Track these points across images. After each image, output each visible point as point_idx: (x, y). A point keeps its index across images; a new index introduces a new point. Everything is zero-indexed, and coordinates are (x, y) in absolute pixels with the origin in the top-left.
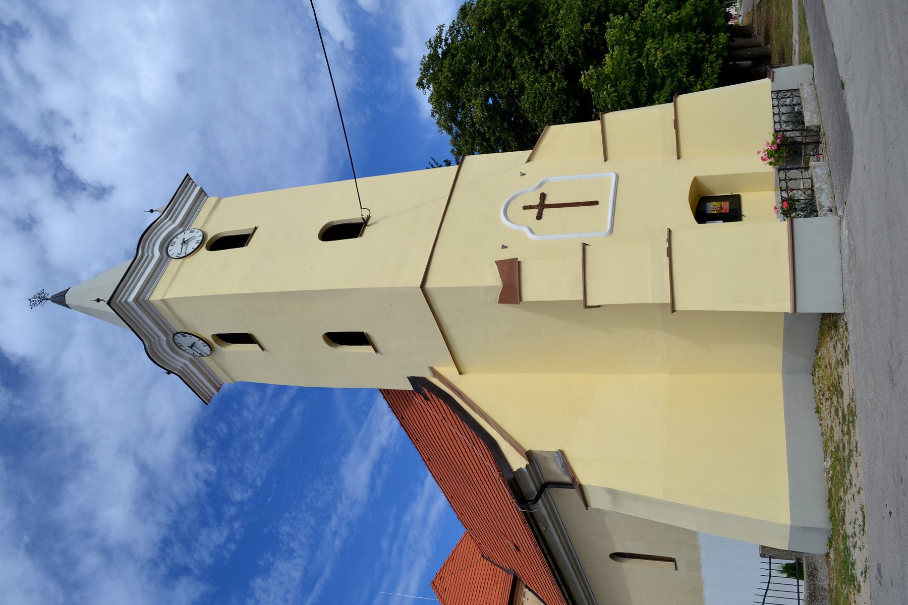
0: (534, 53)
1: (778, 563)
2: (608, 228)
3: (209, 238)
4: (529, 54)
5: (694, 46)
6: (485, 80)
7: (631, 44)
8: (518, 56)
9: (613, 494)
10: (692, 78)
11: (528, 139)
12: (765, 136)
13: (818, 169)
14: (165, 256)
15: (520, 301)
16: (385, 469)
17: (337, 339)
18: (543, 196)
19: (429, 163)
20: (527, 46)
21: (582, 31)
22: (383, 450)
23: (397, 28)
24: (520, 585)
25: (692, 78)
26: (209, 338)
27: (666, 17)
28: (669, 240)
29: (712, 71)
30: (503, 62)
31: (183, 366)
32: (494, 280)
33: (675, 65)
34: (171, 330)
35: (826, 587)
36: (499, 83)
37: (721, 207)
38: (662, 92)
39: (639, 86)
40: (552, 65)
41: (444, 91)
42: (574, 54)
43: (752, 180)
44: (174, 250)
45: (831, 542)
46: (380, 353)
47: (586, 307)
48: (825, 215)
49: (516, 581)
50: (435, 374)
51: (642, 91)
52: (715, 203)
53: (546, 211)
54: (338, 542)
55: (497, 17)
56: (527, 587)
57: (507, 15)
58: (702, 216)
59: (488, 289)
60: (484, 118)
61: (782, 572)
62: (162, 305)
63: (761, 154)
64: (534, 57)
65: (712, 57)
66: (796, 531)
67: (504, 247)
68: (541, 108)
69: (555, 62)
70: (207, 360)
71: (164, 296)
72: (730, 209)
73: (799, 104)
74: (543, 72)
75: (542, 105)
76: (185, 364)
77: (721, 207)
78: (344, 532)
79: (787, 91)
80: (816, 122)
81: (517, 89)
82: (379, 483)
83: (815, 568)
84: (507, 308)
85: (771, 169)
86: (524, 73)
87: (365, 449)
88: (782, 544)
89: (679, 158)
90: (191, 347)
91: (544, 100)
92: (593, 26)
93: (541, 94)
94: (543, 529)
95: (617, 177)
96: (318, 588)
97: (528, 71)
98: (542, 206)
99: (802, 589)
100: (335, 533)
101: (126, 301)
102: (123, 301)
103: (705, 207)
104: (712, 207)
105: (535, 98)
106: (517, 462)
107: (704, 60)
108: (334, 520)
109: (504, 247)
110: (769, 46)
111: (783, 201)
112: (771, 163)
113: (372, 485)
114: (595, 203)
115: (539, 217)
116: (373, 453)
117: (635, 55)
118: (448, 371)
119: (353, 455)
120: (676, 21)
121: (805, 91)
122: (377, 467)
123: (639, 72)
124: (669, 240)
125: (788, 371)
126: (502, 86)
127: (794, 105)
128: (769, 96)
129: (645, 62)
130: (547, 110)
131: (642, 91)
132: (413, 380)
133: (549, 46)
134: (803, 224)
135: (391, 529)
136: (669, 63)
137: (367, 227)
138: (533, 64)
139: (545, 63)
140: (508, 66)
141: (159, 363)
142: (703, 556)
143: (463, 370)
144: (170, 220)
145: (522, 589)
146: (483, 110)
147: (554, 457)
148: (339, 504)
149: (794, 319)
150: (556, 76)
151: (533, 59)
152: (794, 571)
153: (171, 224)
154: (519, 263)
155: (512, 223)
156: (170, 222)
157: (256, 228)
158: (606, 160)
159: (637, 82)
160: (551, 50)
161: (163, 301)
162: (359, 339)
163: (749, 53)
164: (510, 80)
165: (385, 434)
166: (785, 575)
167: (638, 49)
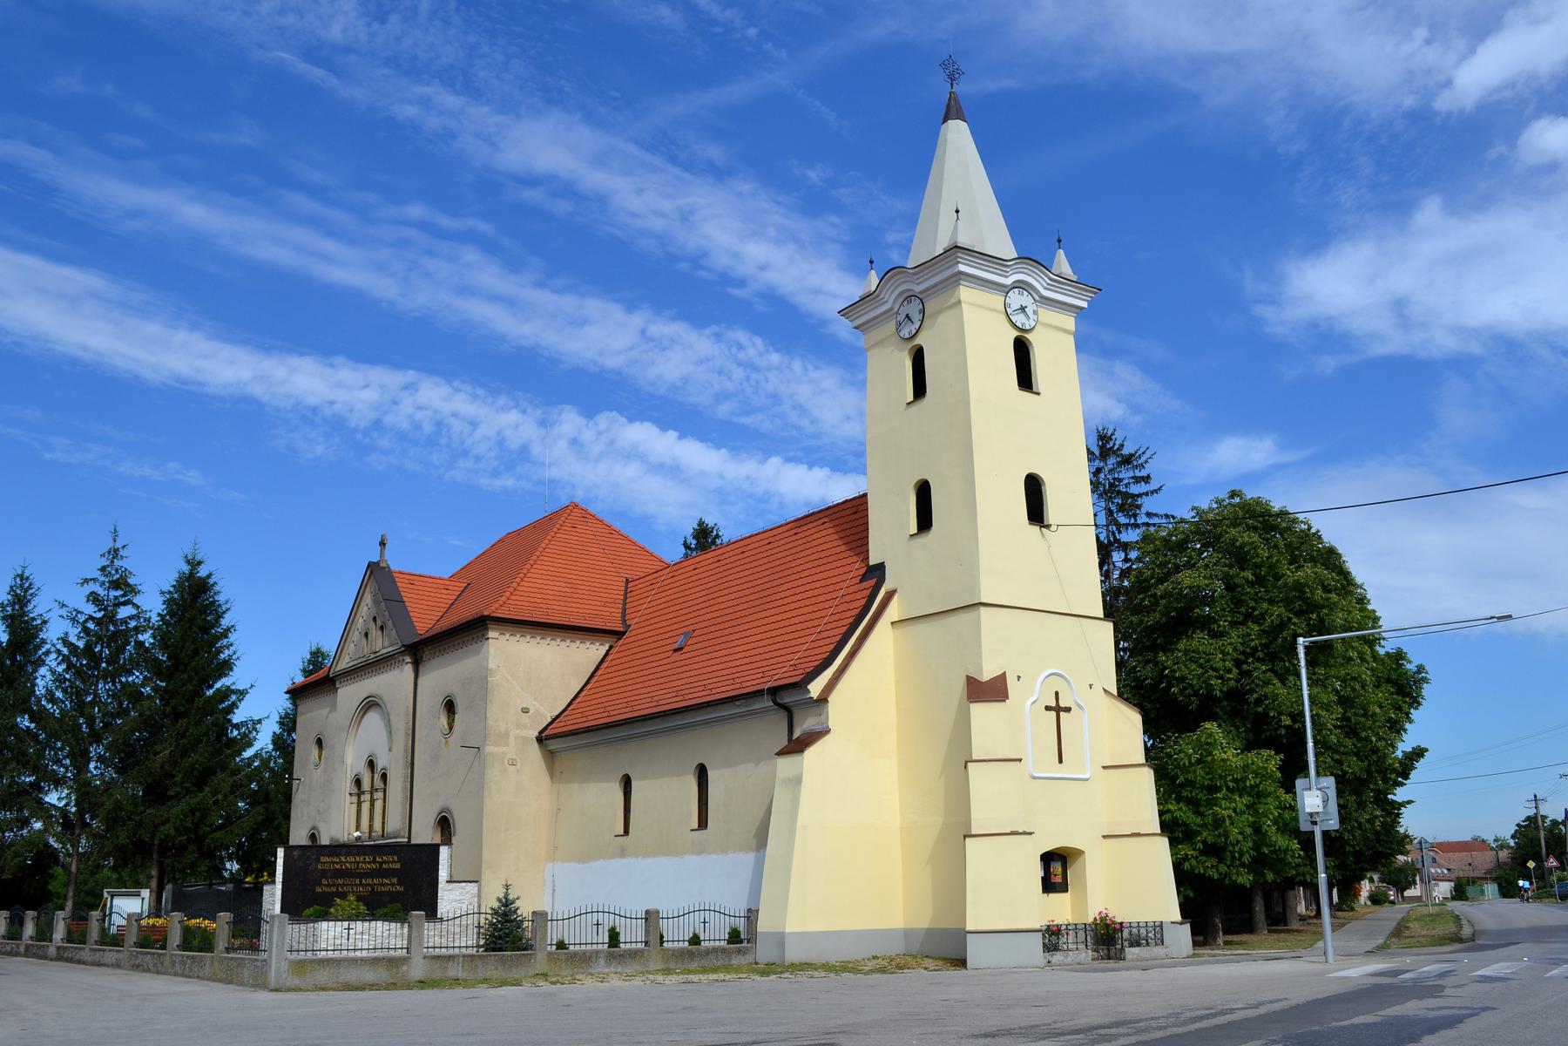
0: (1262, 651)
1: (741, 925)
2: (1037, 775)
3: (1026, 336)
4: (1261, 644)
5: (1237, 849)
6: (1230, 587)
7: (1244, 780)
8: (1260, 630)
9: (797, 781)
10: (1200, 846)
11: (1157, 638)
12: (1122, 913)
13: (1086, 955)
14: (1005, 290)
15: (971, 702)
16: (563, 207)
17: (924, 492)
18: (1068, 710)
19: (1148, 448)
20: (1271, 642)
21: (1281, 713)
22: (601, 200)
23: (1483, 203)
24: (613, 640)
25: (1200, 846)
26: (918, 341)
27: (1269, 819)
28: (1025, 833)
29: (1207, 867)
30: (1254, 609)
31: (885, 300)
32: (987, 674)
33: (1216, 828)
34: (927, 296)
35: (732, 962)
36: (1228, 604)
37: (1056, 875)
38: (1190, 814)
39: (1197, 788)
40: (1248, 674)
41: (1221, 533)
42: (1259, 701)
43: (1081, 901)
44: (1016, 299)
45: (772, 965)
46: (909, 540)
47: (966, 762)
48: (1045, 958)
49: (619, 635)
50: (890, 595)
51: (1191, 792)
52: (1060, 869)
53: (1053, 714)
54: (410, 111)
55: (1308, 604)
56: (611, 647)
57: (1310, 619)
58: (1048, 858)
59: (980, 668)
60: (1181, 588)
61: (731, 928)
62: (953, 301)
63: (1105, 911)
64: (1258, 651)
65: (1223, 868)
66: (780, 939)
67: (1019, 677)
68: (1191, 660)
69: (1250, 677)
70: (890, 327)
71: (965, 303)
72: (1055, 883)
73: (1148, 944)
74: (1238, 663)
75: (1194, 662)
76: (886, 302)
77: (1056, 875)
78: (433, 123)
79: (1162, 936)
80: (1129, 957)
81: (1218, 628)
82: (533, 196)
83: (745, 954)
84: (960, 686)
85: (1090, 920)
86: (1239, 637)
87: (601, 160)
88: (763, 925)
89: (1104, 837)
90: (907, 316)
91: (1201, 666)
92: (1287, 727)
93: (1209, 661)
94: (737, 703)
95: (1087, 780)
96: (317, 73)
97: (1240, 643)
98: (1058, 710)
99: (681, 944)
100: (426, 103)
101: (958, 262)
102: (959, 260)
103: (1057, 861)
104: (1057, 868)
105: (1205, 653)
106: (815, 688)
107: (1221, 860)
108: (452, 101)
109: (1019, 677)
110: (1266, 932)
111: (1057, 926)
112: (1095, 919)
113: (530, 180)
114: (1061, 761)
115: (1048, 708)
116: (595, 179)
117: (1231, 784)
118: (893, 612)
119: (587, 137)
120: (1263, 831)
121: (1160, 950)
122: (568, 189)
123: (1213, 789)
124: (1025, 833)
125: (908, 933)
126: (1224, 610)
127: (1147, 940)
128: (1158, 919)
129: (1221, 796)
130: (1188, 668)
131: (1191, 792)
132: (880, 568)
133: (1269, 670)
134: (1037, 941)
135: (446, 222)
136: (1218, 823)
137: (1039, 528)
138: (1248, 650)
139: (1249, 664)
140: (1248, 616)
141: (887, 276)
142: (714, 856)
143: (895, 626)
144: (1048, 284)
145: (607, 642)
146: (1190, 588)
147: (822, 724)
148: (486, 109)
149: (961, 935)
150: (1230, 679)
151: (1255, 649)
152: (734, 936)
153: (1043, 286)
154: (1005, 701)
155: (1046, 677)
156: (1045, 285)
157: (1038, 394)
158: (1104, 767)
159: (1203, 787)
160: (1264, 672)
161: (959, 302)
162: (925, 521)
163: (1257, 909)
164: (1229, 619)
165: (635, 203)
166: (691, 935)
167: (1238, 788)
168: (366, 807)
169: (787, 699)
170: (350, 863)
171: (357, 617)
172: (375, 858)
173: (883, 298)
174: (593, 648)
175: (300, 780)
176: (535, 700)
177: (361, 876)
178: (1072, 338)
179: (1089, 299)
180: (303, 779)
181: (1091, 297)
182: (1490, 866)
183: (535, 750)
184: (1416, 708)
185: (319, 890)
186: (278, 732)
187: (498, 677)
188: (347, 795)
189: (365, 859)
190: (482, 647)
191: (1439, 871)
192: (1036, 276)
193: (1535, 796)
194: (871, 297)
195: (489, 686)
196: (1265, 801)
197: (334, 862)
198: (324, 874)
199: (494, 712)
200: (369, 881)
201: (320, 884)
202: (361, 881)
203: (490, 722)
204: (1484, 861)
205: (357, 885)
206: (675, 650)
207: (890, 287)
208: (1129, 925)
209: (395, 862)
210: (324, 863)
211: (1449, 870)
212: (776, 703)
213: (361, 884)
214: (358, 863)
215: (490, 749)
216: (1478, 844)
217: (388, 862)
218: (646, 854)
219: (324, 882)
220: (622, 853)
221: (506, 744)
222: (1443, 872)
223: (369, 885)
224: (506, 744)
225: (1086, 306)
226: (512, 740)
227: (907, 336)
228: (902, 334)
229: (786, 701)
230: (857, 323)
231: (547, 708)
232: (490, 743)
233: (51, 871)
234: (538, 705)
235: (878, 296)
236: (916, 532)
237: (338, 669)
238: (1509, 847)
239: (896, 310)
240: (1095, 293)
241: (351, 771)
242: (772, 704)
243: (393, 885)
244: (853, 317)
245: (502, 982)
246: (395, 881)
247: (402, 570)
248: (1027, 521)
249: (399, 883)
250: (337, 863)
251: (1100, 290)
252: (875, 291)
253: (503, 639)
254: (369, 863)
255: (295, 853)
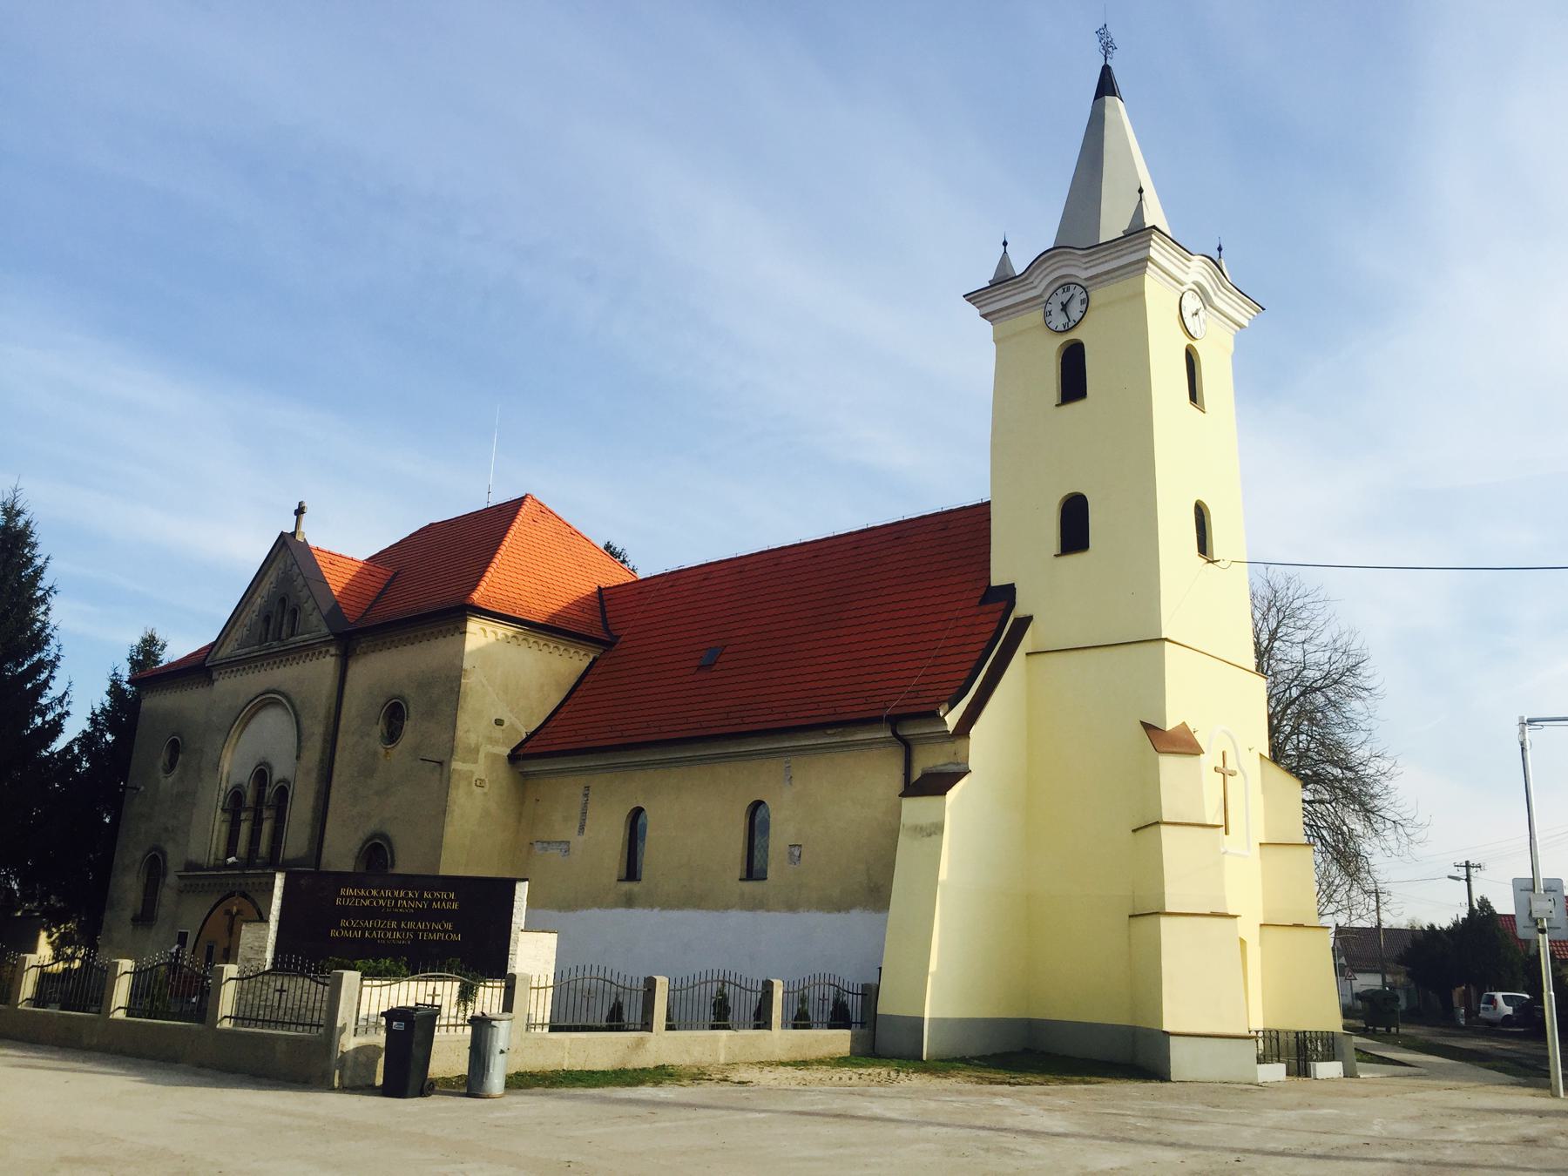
76: (1035, 287)
168: (245, 828)
169: (910, 731)
170: (384, 898)
171: (256, 595)
172: (421, 895)
173: (1032, 282)
175: (138, 789)
176: (511, 711)
177: (400, 917)
179: (1251, 317)
180: (142, 788)
181: (1254, 316)
185: (334, 933)
186: (89, 730)
187: (473, 679)
188: (219, 811)
189: (407, 894)
194: (1014, 281)
195: (462, 689)
197: (361, 897)
198: (346, 912)
199: (464, 721)
200: (411, 925)
201: (338, 927)
202: (399, 925)
203: (460, 733)
205: (392, 930)
206: (700, 668)
207: (1041, 272)
209: (451, 900)
210: (347, 897)
212: (895, 734)
213: (399, 929)
214: (396, 900)
215: (457, 765)
217: (442, 901)
218: (667, 905)
219: (344, 923)
220: (629, 902)
221: (476, 761)
223: (410, 930)
224: (476, 761)
225: (1247, 325)
226: (482, 755)
227: (1061, 328)
228: (1052, 326)
229: (905, 733)
230: (987, 310)
231: (524, 723)
232: (457, 758)
233: (1408, 969)
234: (514, 718)
235: (1026, 279)
236: (1060, 553)
237: (220, 655)
239: (1046, 298)
240: (1257, 312)
241: (228, 782)
242: (891, 735)
243: (445, 931)
244: (982, 303)
245: (593, 1077)
246: (449, 926)
247: (321, 547)
248: (1197, 553)
249: (455, 931)
250: (365, 898)
251: (1263, 309)
252: (1020, 275)
254: (411, 899)
255: (302, 882)
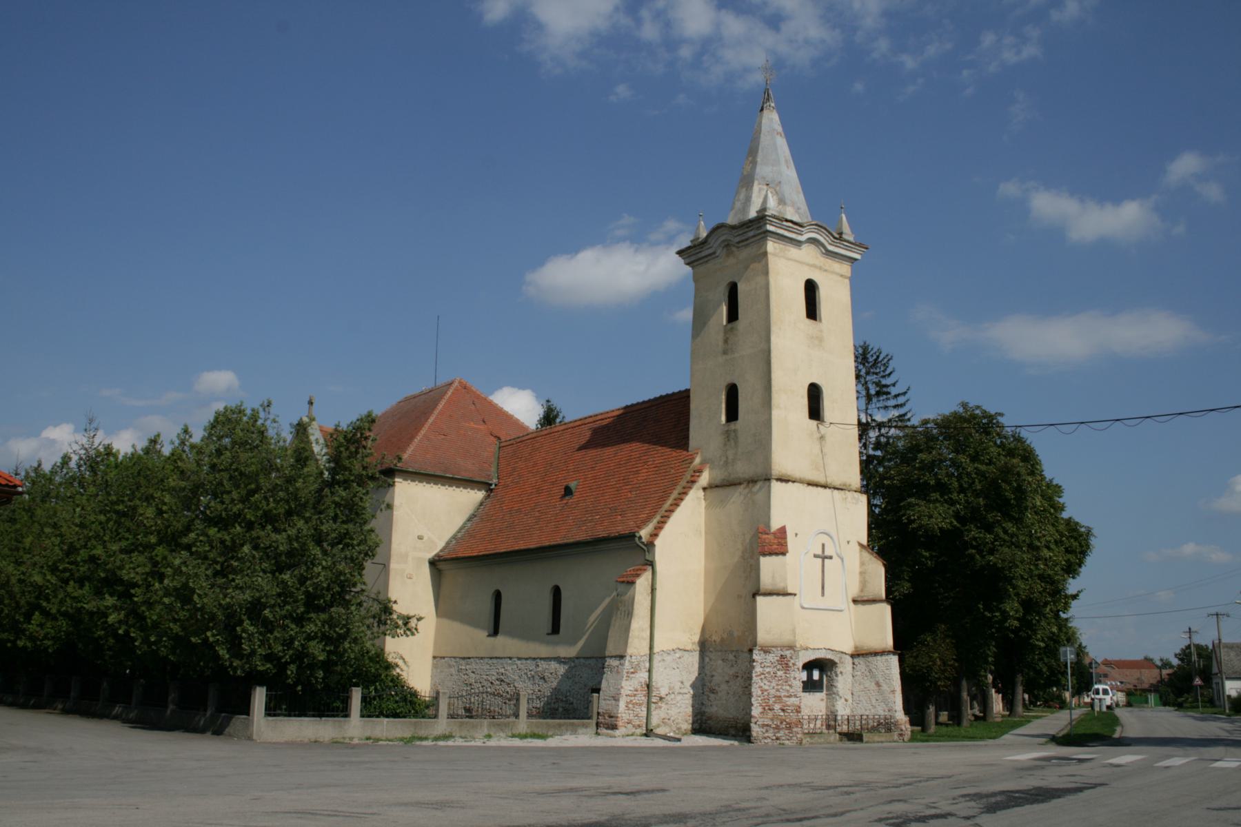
67: (796, 535)
106: (644, 533)
109: (796, 535)
115: (816, 556)
174: (472, 492)
178: (847, 281)
182: (1154, 681)
183: (426, 570)
184: (1073, 578)
190: (387, 493)
191: (1114, 683)
192: (821, 233)
193: (1190, 629)
196: (951, 676)
204: (1149, 677)
208: (807, 717)
211: (1121, 683)
216: (1148, 662)
222: (1116, 685)
231: (437, 542)
238: (1171, 667)
253: (405, 483)
